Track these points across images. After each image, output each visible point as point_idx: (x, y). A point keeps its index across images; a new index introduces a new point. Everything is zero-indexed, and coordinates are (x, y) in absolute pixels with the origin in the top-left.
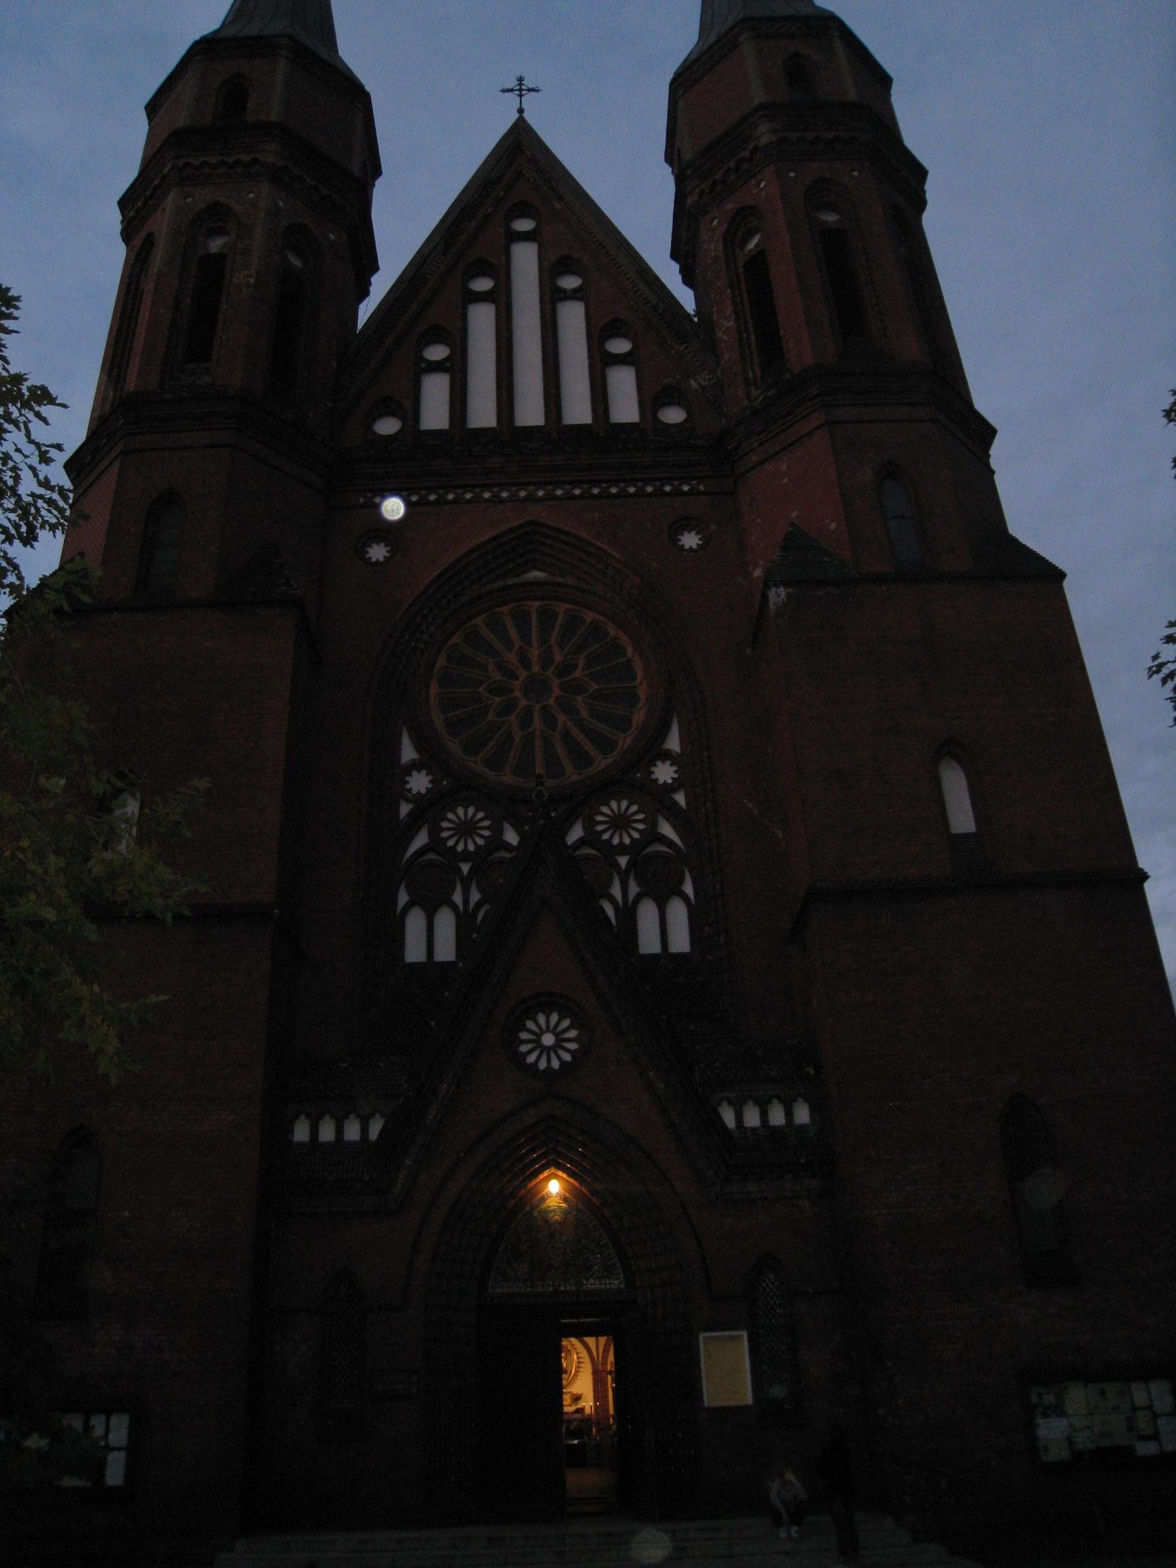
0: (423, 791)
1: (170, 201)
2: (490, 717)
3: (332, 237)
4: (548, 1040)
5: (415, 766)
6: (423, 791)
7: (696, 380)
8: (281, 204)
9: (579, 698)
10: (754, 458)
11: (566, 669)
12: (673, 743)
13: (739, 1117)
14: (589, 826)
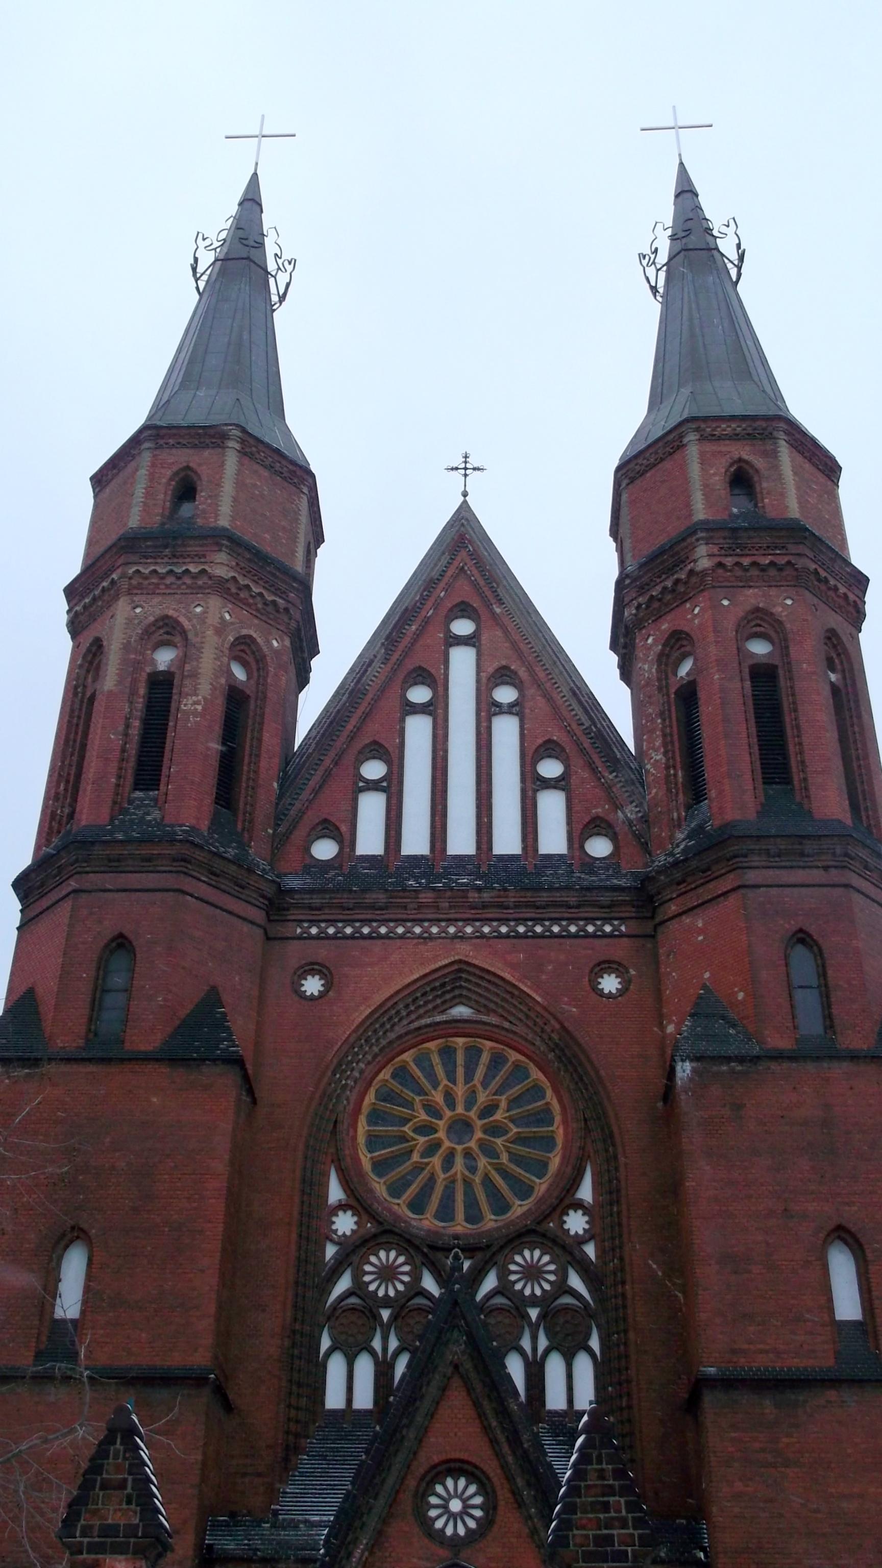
0: (348, 1233)
1: (122, 609)
2: (416, 1157)
3: (275, 644)
4: (456, 1506)
5: (342, 1207)
6: (348, 1233)
7: (623, 813)
8: (227, 617)
9: (498, 1141)
11: (488, 1110)
12: (586, 1192)
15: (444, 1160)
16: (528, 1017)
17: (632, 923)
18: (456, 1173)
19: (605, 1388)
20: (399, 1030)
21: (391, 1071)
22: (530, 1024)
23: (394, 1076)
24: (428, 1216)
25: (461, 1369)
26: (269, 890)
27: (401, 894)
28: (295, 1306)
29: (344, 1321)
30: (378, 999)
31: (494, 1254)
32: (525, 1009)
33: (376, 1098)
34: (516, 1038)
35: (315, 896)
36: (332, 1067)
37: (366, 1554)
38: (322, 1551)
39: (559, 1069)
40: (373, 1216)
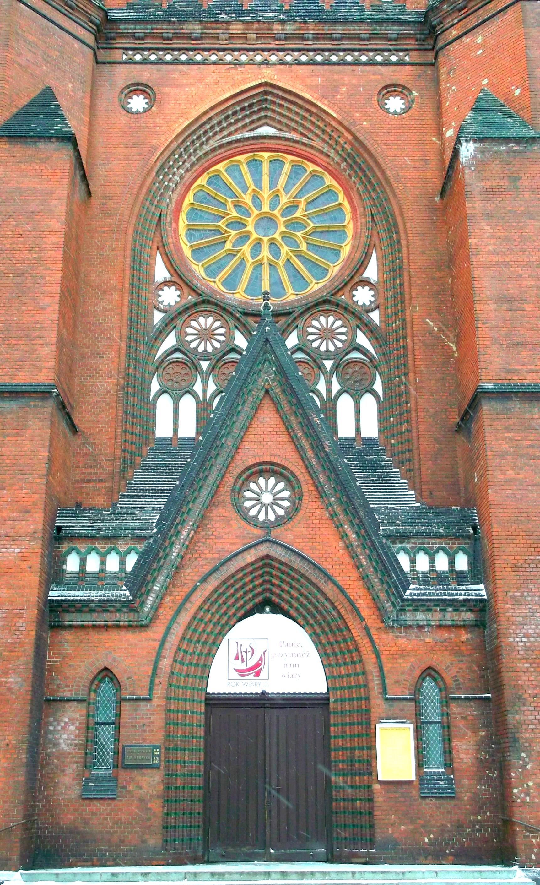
0: (173, 303)
4: (267, 498)
9: (299, 234)
10: (454, 32)
13: (413, 562)
14: (303, 335)
15: (252, 249)
16: (324, 131)
17: (414, 53)
18: (263, 258)
19: (387, 420)
20: (213, 143)
21: (207, 178)
22: (327, 138)
23: (209, 182)
24: (240, 290)
25: (271, 392)
26: (97, 17)
27: (214, 25)
28: (128, 355)
29: (171, 371)
30: (195, 114)
31: (295, 319)
32: (322, 125)
33: (194, 200)
34: (313, 152)
35: (138, 27)
36: (156, 169)
37: (192, 532)
38: (155, 530)
39: (350, 176)
40: (193, 290)
